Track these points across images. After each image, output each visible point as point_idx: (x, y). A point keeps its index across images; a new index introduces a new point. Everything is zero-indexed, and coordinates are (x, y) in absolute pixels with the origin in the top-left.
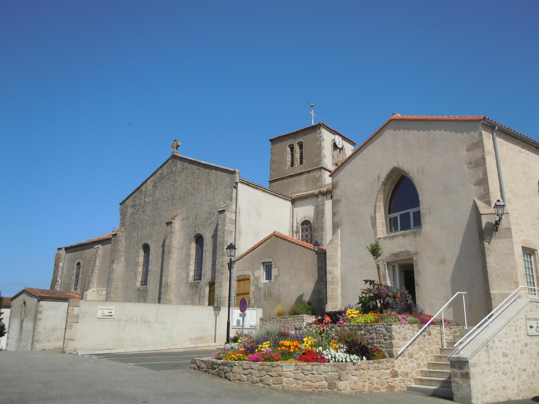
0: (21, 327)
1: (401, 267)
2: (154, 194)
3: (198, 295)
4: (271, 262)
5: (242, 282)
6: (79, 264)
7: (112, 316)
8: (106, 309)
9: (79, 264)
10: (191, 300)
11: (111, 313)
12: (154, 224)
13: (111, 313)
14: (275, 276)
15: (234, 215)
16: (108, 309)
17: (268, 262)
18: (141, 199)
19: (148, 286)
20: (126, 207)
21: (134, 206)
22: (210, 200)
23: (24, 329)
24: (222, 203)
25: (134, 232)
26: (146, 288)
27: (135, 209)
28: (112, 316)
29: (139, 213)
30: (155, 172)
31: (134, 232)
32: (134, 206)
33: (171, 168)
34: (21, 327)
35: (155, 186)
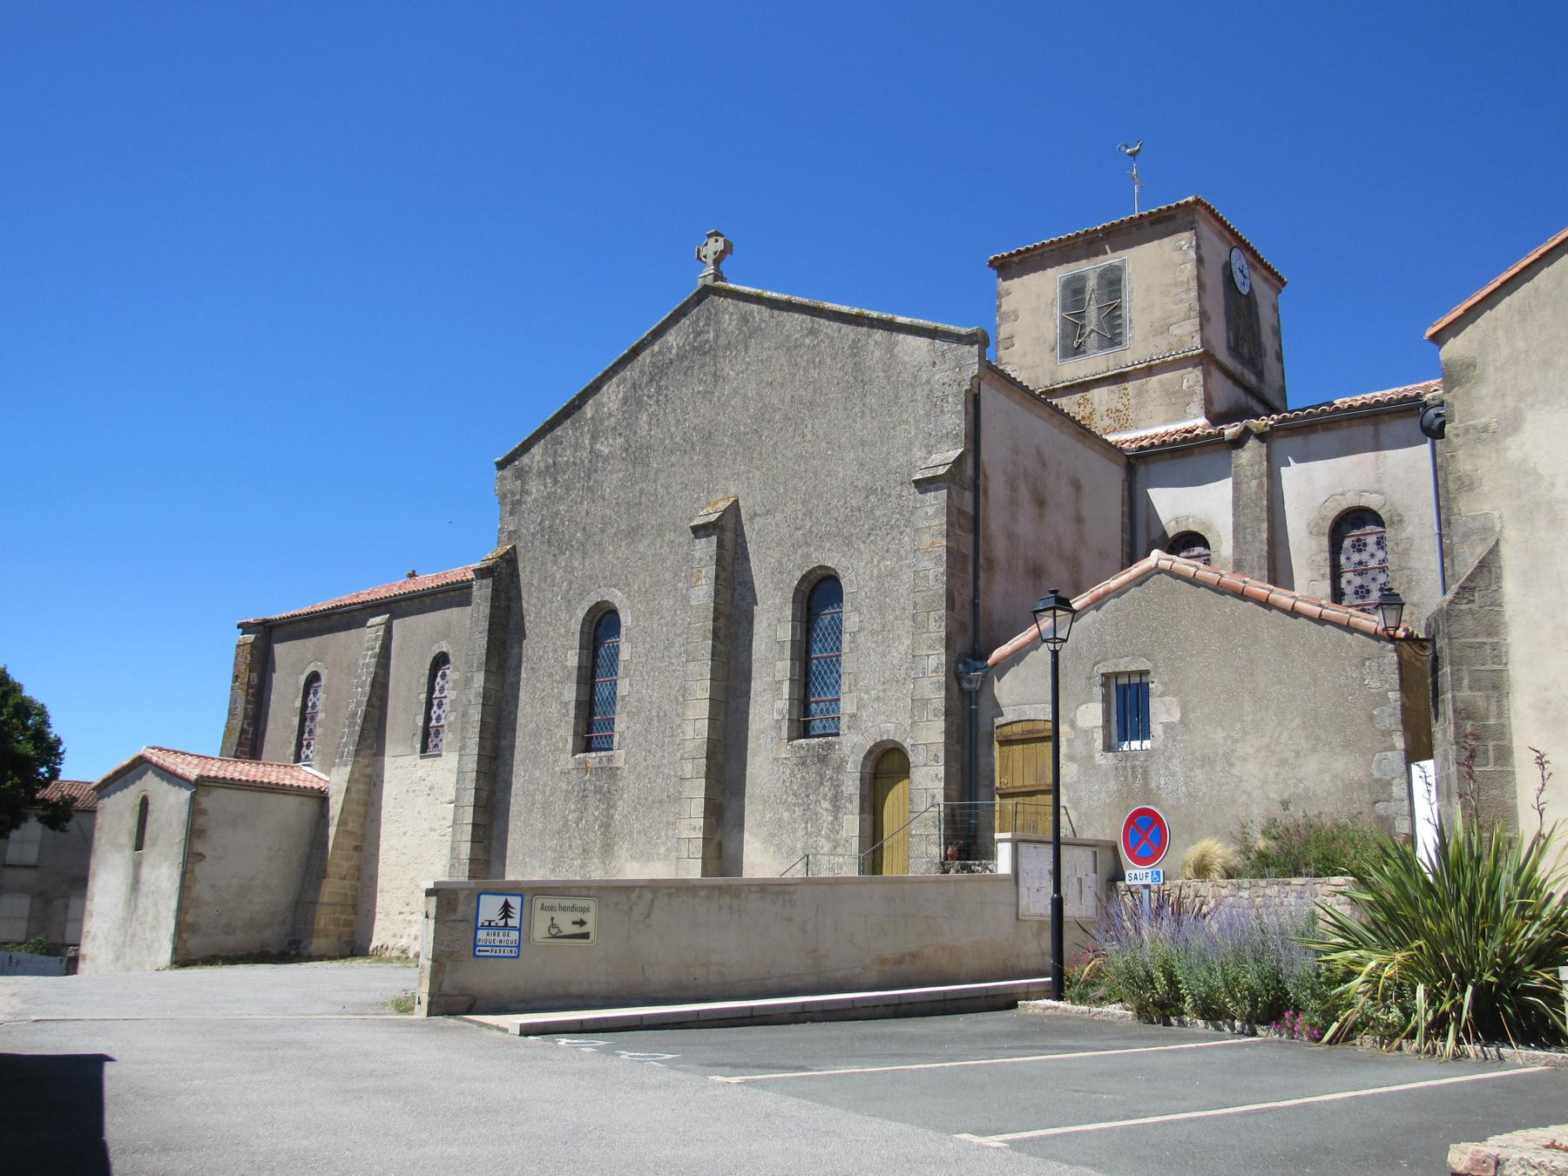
0: (135, 884)
1: (1123, 691)
2: (630, 423)
3: (826, 789)
4: (1147, 672)
5: (1018, 748)
6: (314, 678)
7: (586, 936)
8: (563, 909)
9: (314, 678)
10: (798, 811)
11: (582, 923)
12: (633, 533)
13: (582, 923)
14: (1168, 727)
15: (968, 496)
16: (573, 909)
17: (1129, 674)
18: (577, 447)
19: (619, 756)
20: (521, 474)
21: (552, 471)
22: (863, 443)
23: (143, 888)
24: (918, 453)
25: (555, 562)
26: (610, 760)
27: (556, 481)
28: (586, 936)
29: (573, 494)
30: (635, 352)
31: (555, 562)
32: (552, 471)
33: (699, 334)
34: (135, 884)
35: (633, 401)
